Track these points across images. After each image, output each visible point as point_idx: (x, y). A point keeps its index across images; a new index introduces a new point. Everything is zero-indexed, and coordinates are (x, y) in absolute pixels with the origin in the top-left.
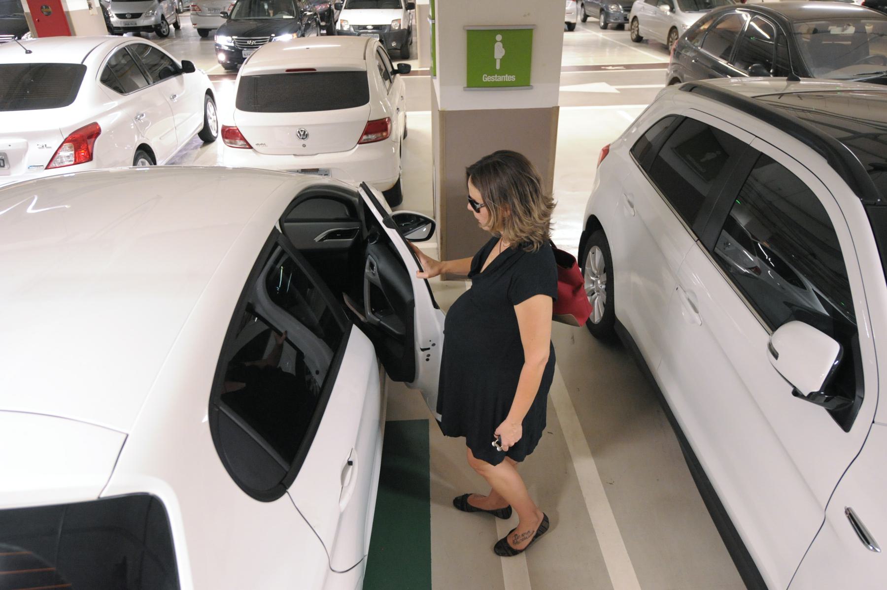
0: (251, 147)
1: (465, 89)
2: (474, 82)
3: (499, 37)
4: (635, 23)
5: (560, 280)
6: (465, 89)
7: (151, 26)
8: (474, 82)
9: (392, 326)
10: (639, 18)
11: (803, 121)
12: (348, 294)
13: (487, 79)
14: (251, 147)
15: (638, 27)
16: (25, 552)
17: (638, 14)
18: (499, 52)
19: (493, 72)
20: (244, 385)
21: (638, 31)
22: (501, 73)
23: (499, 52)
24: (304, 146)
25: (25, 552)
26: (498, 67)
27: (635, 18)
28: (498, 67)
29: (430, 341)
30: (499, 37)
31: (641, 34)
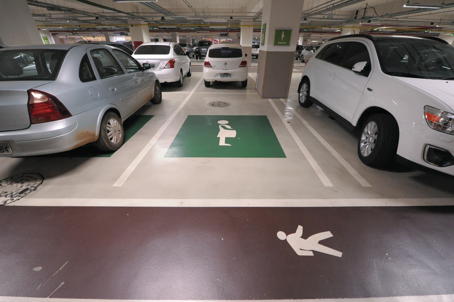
0: (212, 67)
1: (273, 46)
2: (276, 44)
3: (283, 32)
4: (302, 56)
5: (372, 149)
6: (273, 46)
7: (210, 82)
8: (276, 44)
9: (132, 48)
10: (304, 56)
11: (371, 129)
12: (68, 262)
13: (279, 43)
14: (212, 67)
15: (303, 57)
16: (426, 62)
17: (303, 54)
18: (283, 36)
19: (281, 41)
20: (231, 145)
21: (303, 59)
22: (283, 41)
23: (283, 36)
24: (225, 67)
25: (426, 62)
26: (282, 40)
27: (303, 55)
28: (282, 40)
29: (39, 29)
30: (283, 32)
31: (304, 59)
